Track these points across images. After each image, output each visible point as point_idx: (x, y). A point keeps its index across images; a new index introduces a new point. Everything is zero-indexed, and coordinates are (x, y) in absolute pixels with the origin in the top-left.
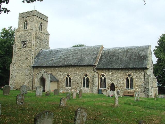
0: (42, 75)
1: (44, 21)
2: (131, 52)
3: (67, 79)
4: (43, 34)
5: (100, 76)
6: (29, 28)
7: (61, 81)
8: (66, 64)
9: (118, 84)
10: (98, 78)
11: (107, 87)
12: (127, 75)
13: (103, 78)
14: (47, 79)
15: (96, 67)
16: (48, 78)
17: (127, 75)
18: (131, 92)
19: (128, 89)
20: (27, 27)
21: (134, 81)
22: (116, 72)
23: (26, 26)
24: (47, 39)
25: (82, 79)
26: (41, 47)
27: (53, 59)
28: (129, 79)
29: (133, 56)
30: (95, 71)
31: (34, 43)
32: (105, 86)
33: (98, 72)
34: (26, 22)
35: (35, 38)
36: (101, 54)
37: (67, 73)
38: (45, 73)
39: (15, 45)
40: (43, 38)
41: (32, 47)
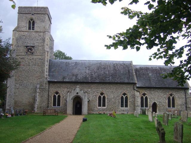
14: (85, 98)
28: (171, 98)
37: (101, 90)
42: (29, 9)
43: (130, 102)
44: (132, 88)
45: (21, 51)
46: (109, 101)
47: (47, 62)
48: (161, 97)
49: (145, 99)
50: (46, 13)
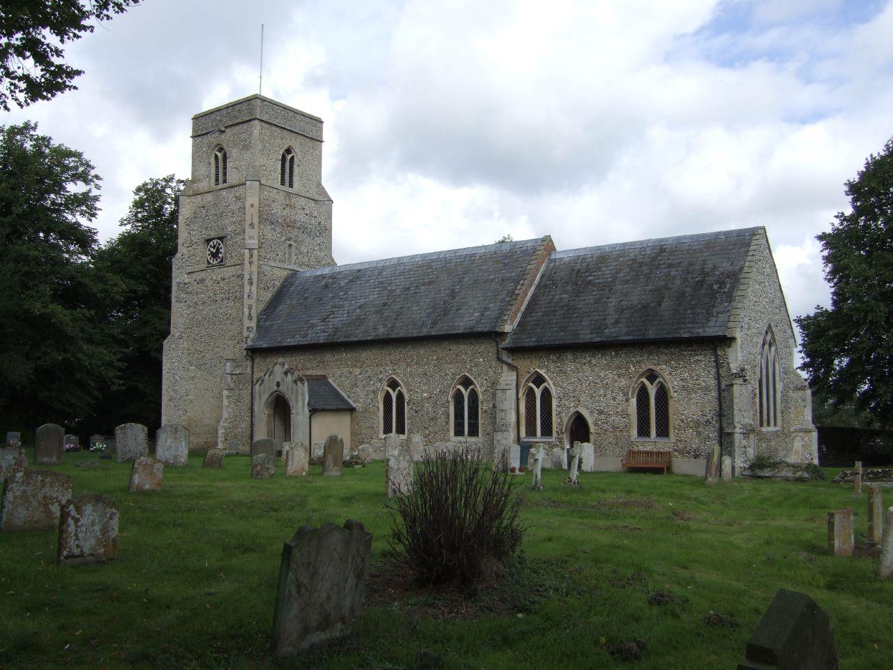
0: (278, 384)
1: (300, 139)
2: (670, 266)
3: (388, 398)
4: (302, 202)
5: (523, 381)
6: (233, 177)
7: (366, 411)
8: (382, 331)
9: (603, 417)
10: (517, 394)
11: (554, 434)
12: (641, 376)
13: (538, 392)
14: (297, 401)
15: (506, 343)
16: (300, 397)
17: (641, 376)
18: (658, 453)
19: (647, 439)
20: (225, 174)
21: (671, 403)
22: (594, 361)
23: (221, 170)
24: (322, 219)
25: (450, 399)
26: (294, 257)
27: (333, 313)
28: (652, 390)
29: (678, 282)
30: (503, 362)
31: (254, 243)
32: (547, 431)
33: (515, 363)
34: (221, 150)
35: (256, 221)
36: (538, 279)
37: (388, 372)
38: (289, 375)
39: (178, 255)
40: (301, 217)
41: (246, 262)
42: (213, 116)
43: (484, 414)
44: (493, 350)
45: (198, 258)
46: (416, 412)
47: (251, 284)
48: (606, 386)
49: (469, 399)
50: (254, 117)
